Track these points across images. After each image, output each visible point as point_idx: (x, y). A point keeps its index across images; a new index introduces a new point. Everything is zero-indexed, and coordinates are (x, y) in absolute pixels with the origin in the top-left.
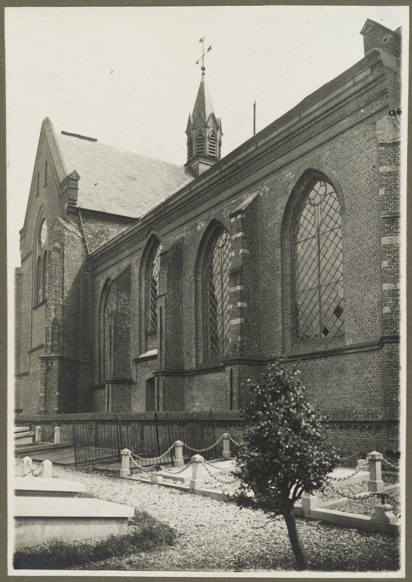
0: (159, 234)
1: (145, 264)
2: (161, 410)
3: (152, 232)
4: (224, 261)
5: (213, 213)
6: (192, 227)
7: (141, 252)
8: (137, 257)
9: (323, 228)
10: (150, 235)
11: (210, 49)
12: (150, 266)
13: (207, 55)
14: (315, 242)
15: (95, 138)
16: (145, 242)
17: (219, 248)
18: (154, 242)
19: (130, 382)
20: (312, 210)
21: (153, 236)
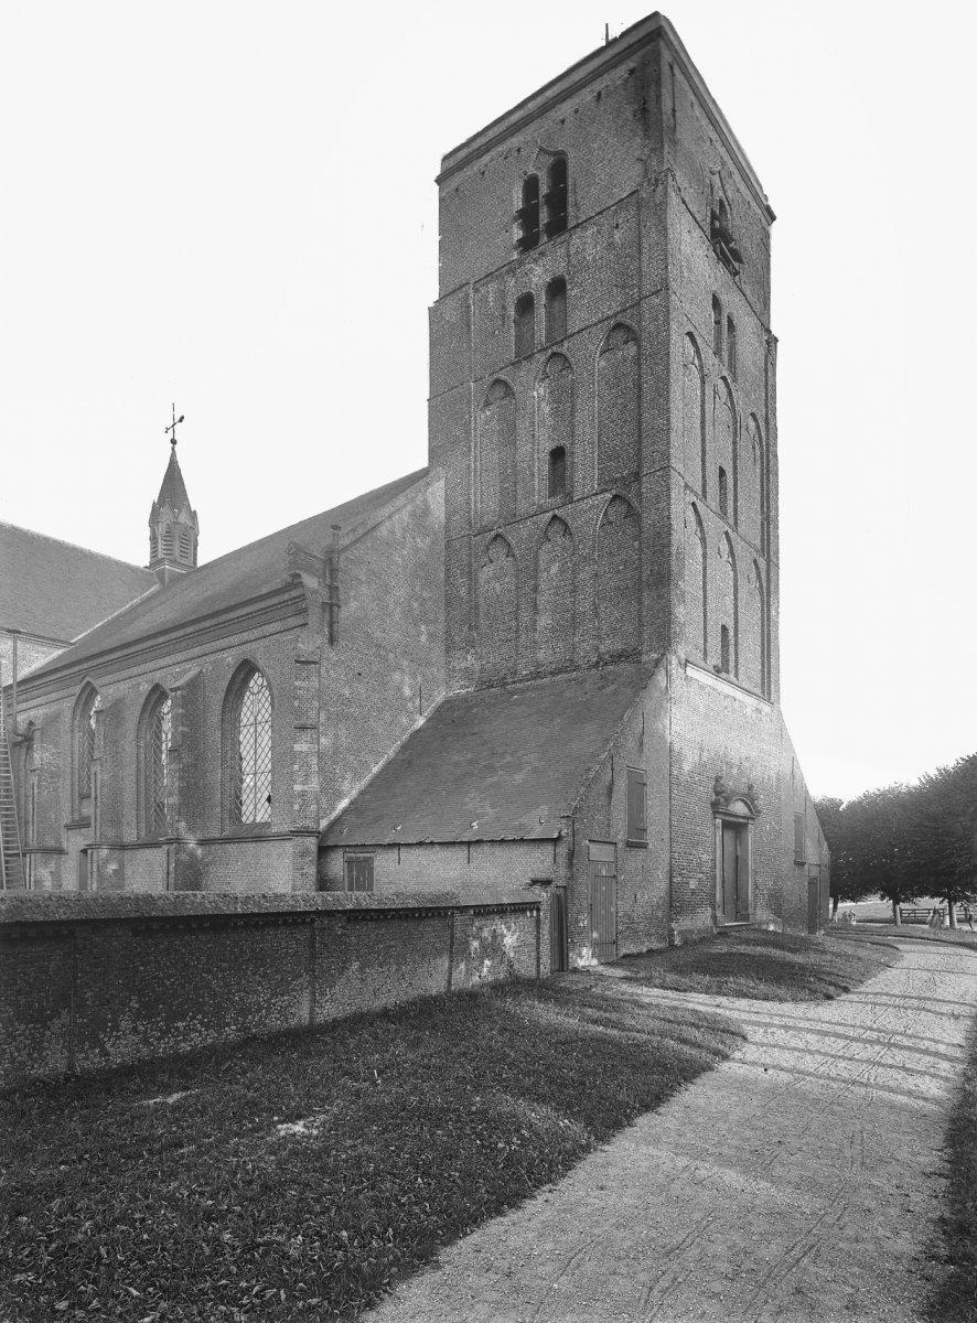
0: (96, 683)
1: (79, 713)
2: (33, 888)
3: (88, 679)
4: (259, 712)
5: (158, 674)
6: (134, 686)
7: (74, 698)
8: (69, 704)
9: (259, 718)
10: (84, 682)
11: (181, 419)
12: (85, 715)
13: (178, 424)
14: (252, 730)
15: (776, 213)
16: (77, 690)
17: (253, 694)
18: (90, 692)
19: (60, 851)
20: (251, 697)
21: (89, 683)
